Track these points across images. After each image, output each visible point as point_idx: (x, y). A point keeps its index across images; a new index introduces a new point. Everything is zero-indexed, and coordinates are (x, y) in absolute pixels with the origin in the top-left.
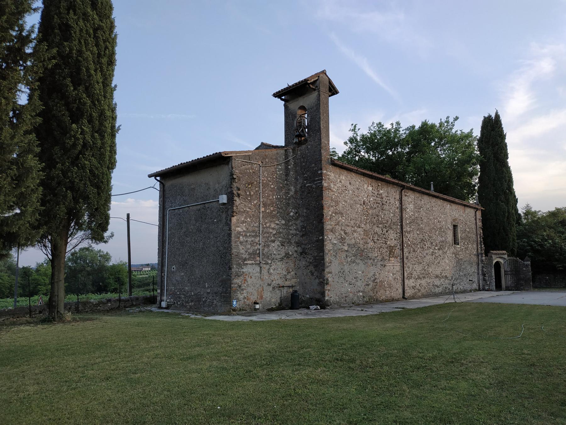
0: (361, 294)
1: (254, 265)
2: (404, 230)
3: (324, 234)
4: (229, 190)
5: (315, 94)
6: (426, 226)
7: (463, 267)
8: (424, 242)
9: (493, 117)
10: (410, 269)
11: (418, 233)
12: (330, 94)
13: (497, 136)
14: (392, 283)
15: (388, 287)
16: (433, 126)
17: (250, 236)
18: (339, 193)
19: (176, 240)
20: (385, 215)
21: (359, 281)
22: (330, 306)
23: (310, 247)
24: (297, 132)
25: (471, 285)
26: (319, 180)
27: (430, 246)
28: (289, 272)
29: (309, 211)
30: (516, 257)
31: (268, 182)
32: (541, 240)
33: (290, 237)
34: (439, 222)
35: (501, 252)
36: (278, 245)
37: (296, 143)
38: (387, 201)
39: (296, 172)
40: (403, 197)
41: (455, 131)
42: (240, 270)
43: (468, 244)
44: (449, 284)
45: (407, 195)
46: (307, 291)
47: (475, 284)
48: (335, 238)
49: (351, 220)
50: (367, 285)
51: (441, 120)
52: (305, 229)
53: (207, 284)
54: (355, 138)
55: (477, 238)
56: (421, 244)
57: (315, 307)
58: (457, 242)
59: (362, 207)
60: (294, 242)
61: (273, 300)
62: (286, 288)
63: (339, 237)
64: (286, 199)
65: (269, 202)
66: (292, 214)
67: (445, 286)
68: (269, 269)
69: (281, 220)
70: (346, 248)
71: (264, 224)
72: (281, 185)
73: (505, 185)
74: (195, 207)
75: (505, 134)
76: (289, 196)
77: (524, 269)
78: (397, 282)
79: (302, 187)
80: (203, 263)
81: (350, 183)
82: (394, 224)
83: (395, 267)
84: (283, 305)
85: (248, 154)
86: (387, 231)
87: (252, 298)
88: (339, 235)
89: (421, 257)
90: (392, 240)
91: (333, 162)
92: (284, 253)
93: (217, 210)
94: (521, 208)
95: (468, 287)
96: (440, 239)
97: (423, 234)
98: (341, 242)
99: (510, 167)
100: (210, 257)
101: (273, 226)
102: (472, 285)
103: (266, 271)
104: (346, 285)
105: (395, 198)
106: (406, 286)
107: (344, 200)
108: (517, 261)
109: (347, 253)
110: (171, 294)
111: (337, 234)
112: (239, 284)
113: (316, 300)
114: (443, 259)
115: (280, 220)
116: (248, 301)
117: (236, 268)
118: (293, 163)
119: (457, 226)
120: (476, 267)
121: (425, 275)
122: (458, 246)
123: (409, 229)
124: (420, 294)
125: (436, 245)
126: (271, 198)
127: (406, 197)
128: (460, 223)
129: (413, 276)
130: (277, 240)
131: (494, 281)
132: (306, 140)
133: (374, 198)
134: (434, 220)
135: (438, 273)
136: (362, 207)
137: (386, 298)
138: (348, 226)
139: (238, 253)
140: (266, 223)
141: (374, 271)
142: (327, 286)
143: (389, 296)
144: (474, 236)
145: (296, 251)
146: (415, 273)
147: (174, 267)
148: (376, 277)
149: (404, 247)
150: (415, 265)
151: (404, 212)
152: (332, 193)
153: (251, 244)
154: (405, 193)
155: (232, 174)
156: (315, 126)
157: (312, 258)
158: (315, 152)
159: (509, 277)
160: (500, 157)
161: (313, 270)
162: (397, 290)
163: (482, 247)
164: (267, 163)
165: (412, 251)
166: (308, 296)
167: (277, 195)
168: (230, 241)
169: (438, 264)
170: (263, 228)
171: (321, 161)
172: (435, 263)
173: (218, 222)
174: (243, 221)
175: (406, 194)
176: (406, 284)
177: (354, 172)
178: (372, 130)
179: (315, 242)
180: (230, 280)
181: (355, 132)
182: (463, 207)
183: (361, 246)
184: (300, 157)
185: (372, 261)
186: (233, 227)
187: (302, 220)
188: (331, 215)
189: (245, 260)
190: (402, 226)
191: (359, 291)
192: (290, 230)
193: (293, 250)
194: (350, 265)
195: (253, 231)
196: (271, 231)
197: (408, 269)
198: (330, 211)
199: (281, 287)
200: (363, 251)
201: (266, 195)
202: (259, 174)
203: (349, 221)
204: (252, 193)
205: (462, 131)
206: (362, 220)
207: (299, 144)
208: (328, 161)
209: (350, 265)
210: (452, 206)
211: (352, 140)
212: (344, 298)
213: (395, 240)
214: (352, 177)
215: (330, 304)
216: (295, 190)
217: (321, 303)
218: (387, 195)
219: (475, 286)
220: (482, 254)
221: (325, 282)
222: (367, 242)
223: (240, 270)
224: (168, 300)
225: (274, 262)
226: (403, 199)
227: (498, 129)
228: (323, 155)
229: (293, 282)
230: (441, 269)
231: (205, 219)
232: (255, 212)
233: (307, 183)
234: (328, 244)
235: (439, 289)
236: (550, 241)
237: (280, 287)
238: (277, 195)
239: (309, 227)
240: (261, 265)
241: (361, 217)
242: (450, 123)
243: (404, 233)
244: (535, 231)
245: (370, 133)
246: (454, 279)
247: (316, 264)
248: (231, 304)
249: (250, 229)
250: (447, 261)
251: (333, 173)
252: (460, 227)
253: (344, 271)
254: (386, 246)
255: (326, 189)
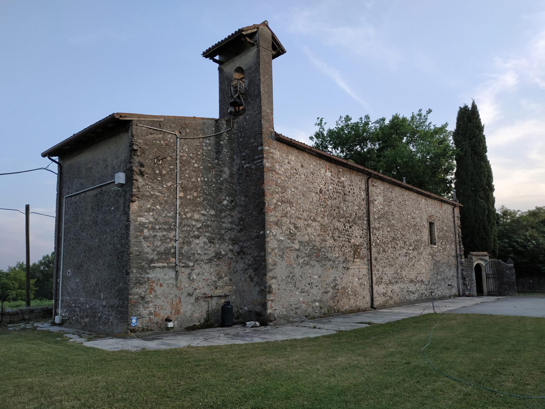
0: (317, 304)
1: (167, 269)
2: (372, 226)
3: (265, 228)
4: (128, 166)
5: (253, 51)
6: (398, 222)
7: (441, 270)
8: (396, 241)
9: (469, 108)
10: (380, 273)
11: (389, 230)
12: (274, 53)
13: (474, 128)
14: (358, 289)
15: (352, 295)
16: (404, 120)
17: (160, 229)
18: (287, 176)
19: (72, 236)
20: (348, 207)
21: (315, 287)
22: (274, 322)
23: (249, 245)
24: (232, 99)
25: (450, 290)
26: (259, 159)
27: (403, 245)
28: (220, 278)
29: (248, 199)
30: (498, 258)
31: (189, 159)
32: (524, 240)
33: (223, 232)
34: (413, 218)
35: (481, 253)
36: (204, 242)
37: (231, 113)
38: (351, 191)
39: (232, 149)
40: (370, 187)
41: (429, 123)
42: (143, 276)
43: (446, 244)
44: (426, 290)
45: (376, 185)
46: (245, 301)
47: (454, 289)
48: (281, 233)
49: (303, 211)
50: (325, 292)
51: (413, 113)
52: (243, 222)
53: (102, 294)
54: (321, 132)
55: (456, 238)
56: (392, 243)
57: (252, 323)
58: (434, 241)
59: (318, 196)
60: (229, 238)
61: (196, 315)
62: (215, 299)
63: (287, 232)
64: (216, 183)
65: (190, 185)
66: (225, 202)
67: (421, 292)
68: (190, 274)
69: (209, 209)
70: (297, 247)
71: (182, 213)
72: (210, 165)
73: (485, 181)
74: (92, 192)
75: (483, 125)
76: (221, 179)
77: (508, 272)
78: (364, 289)
79: (241, 168)
80: (99, 266)
81: (302, 166)
82: (359, 218)
83: (361, 270)
84: (211, 321)
85: (159, 120)
86: (350, 227)
87: (162, 314)
88: (286, 230)
89: (393, 258)
90: (357, 237)
91: (278, 136)
92: (214, 253)
93: (114, 195)
94: (498, 206)
95: (447, 292)
96: (414, 237)
97: (394, 232)
98: (289, 239)
99: (489, 161)
100: (106, 259)
101: (196, 216)
102: (451, 290)
103: (185, 276)
104: (297, 293)
105: (360, 188)
106: (374, 293)
107: (294, 186)
108: (499, 263)
109: (298, 253)
110: (66, 307)
111: (284, 228)
112: (141, 294)
113: (256, 314)
114: (418, 260)
115: (207, 210)
116: (156, 318)
117: (137, 272)
118: (227, 138)
119: (433, 223)
120: (456, 270)
121: (397, 279)
122: (435, 246)
123: (377, 225)
124: (392, 302)
125: (410, 244)
126: (194, 180)
127: (374, 187)
128: (436, 220)
129: (383, 281)
130: (203, 236)
131: (475, 285)
132: (244, 110)
133: (334, 186)
134: (407, 216)
135: (413, 277)
136: (318, 196)
137: (350, 308)
138: (300, 218)
139: (140, 252)
140: (187, 212)
141: (334, 276)
142: (270, 295)
143: (354, 305)
144: (452, 235)
145: (231, 250)
146: (385, 277)
147: (69, 271)
148: (337, 282)
149: (372, 247)
150: (386, 268)
151: (371, 205)
152: (277, 176)
153: (161, 240)
154: (372, 182)
155: (132, 144)
156: (254, 90)
157: (252, 258)
158: (254, 123)
159: (491, 281)
160: (478, 150)
161: (253, 274)
162: (364, 297)
163: (461, 248)
164: (188, 134)
165: (381, 251)
166: (246, 308)
167: (202, 176)
168: (127, 235)
169: (412, 267)
170: (182, 219)
171: (261, 133)
172: (409, 266)
173: (115, 210)
174: (150, 208)
175: (373, 183)
176: (375, 290)
177: (307, 153)
178: (339, 125)
179: (255, 239)
180: (127, 289)
181: (321, 126)
182: (439, 203)
183: (318, 244)
184: (236, 132)
185: (331, 262)
186: (132, 217)
187: (240, 210)
188: (276, 204)
189: (152, 261)
190: (369, 221)
191: (315, 301)
192: (223, 223)
193: (227, 249)
194: (301, 267)
195: (165, 223)
196: (194, 223)
197: (377, 273)
198: (274, 198)
199: (206, 297)
200: (320, 250)
201: (187, 175)
202: (175, 147)
203: (301, 212)
204: (164, 172)
205: (436, 126)
206: (318, 212)
207: (236, 114)
208: (271, 134)
209: (301, 267)
210: (427, 201)
211: (318, 135)
212: (294, 310)
213: (361, 237)
214: (305, 158)
215: (272, 319)
216: (231, 172)
217: (262, 318)
218: (350, 184)
219: (454, 291)
220: (461, 255)
221: (267, 290)
222: (324, 239)
223: (143, 276)
224: (63, 314)
225: (199, 264)
226: (370, 190)
227: (476, 120)
228: (264, 126)
229: (226, 290)
230: (417, 272)
231: (102, 207)
232: (169, 197)
233: (245, 164)
234: (271, 241)
235: (414, 295)
236: (534, 242)
237: (206, 297)
238: (202, 176)
239: (248, 220)
240: (178, 268)
241: (317, 208)
242: (423, 116)
243: (371, 229)
244: (516, 231)
245: (338, 127)
246: (431, 284)
247: (256, 266)
248: (128, 323)
249: (161, 219)
250: (423, 263)
251: (279, 151)
252: (436, 225)
253: (293, 276)
254: (350, 244)
255: (268, 171)
